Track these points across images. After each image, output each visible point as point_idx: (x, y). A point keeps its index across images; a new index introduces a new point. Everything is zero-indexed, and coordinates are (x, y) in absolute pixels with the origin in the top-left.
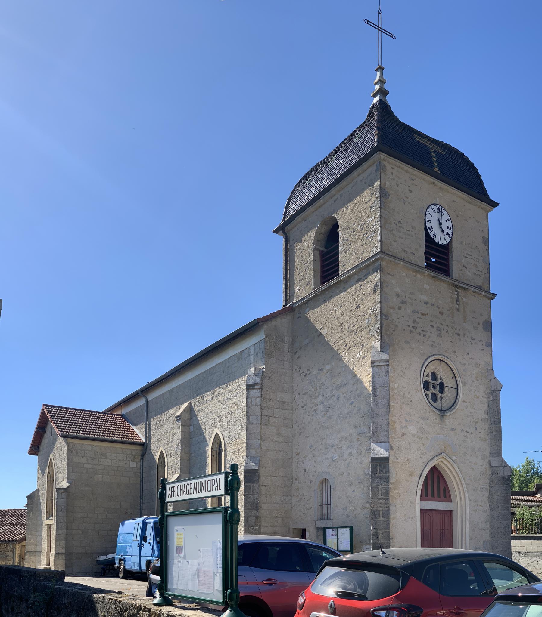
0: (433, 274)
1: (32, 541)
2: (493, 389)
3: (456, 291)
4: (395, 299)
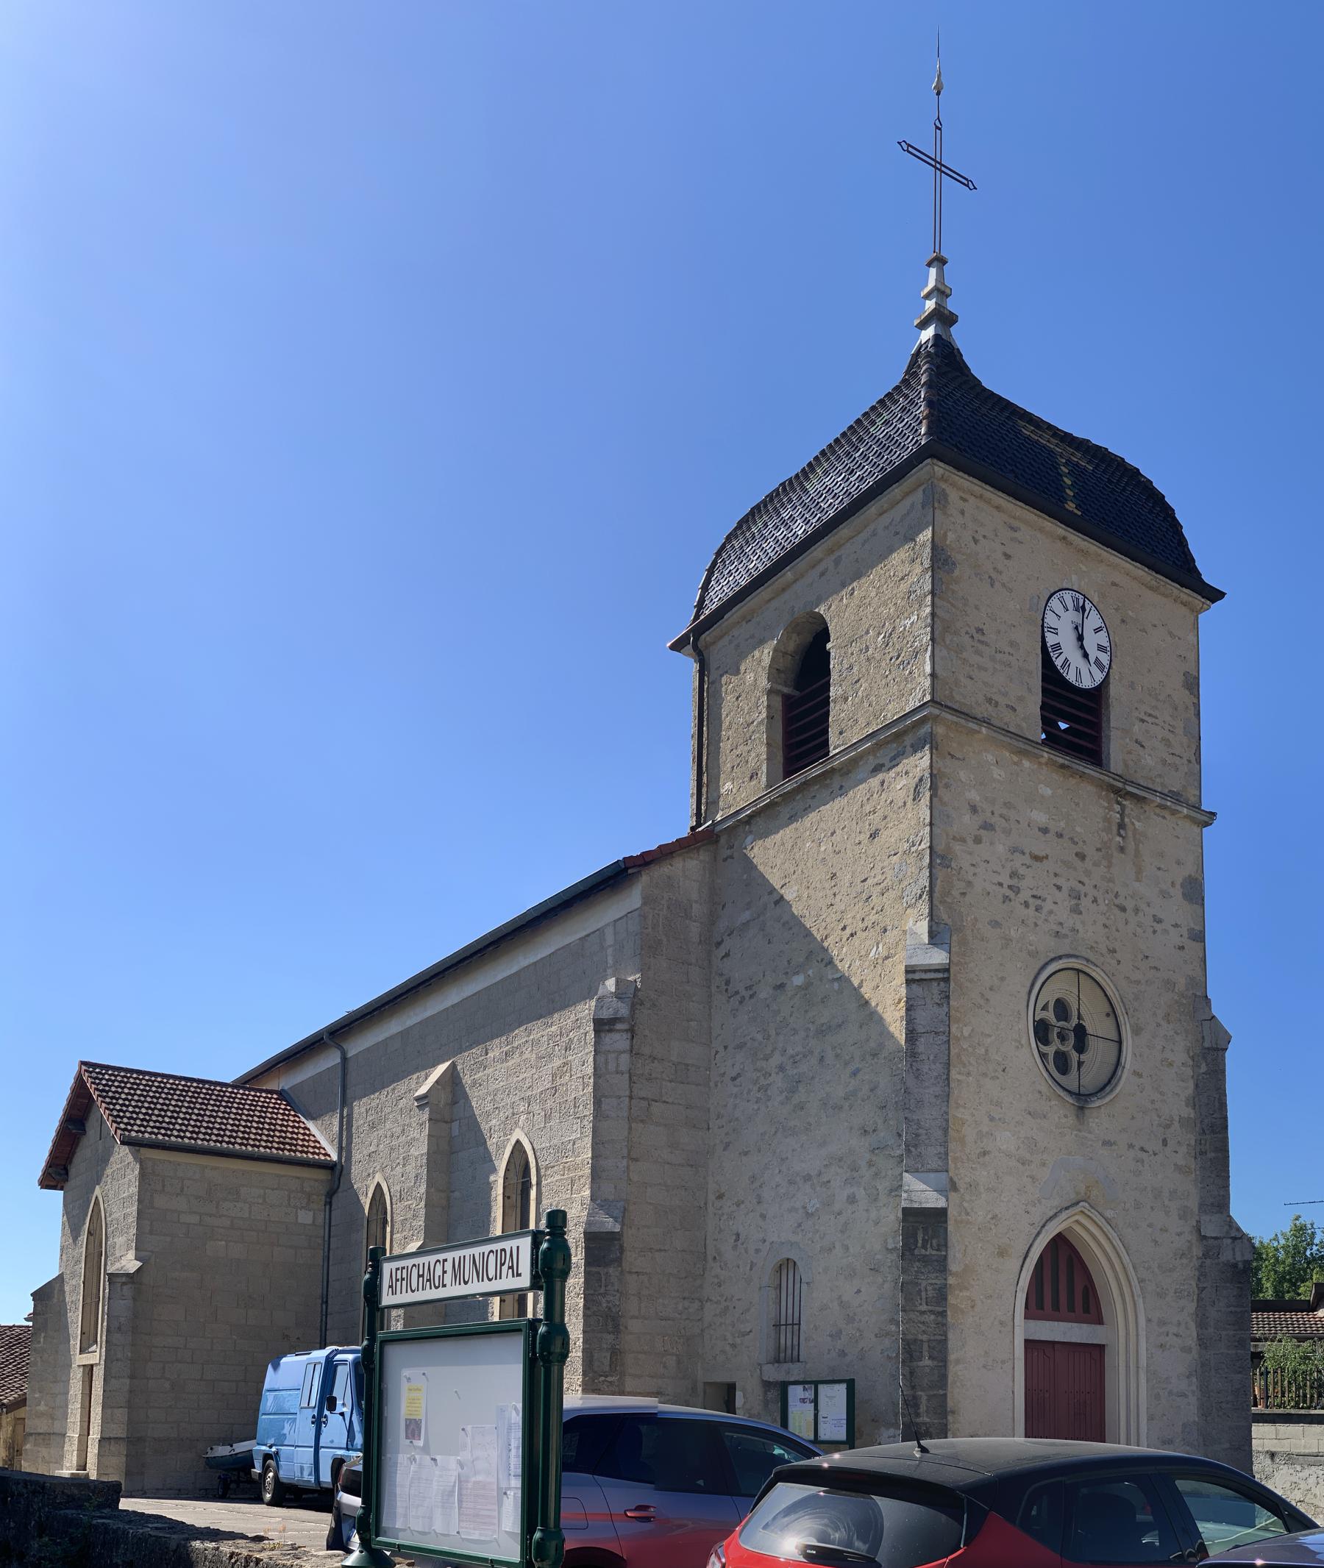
1: (42, 1408)
2: (1207, 1045)
3: (1118, 803)
4: (967, 818)
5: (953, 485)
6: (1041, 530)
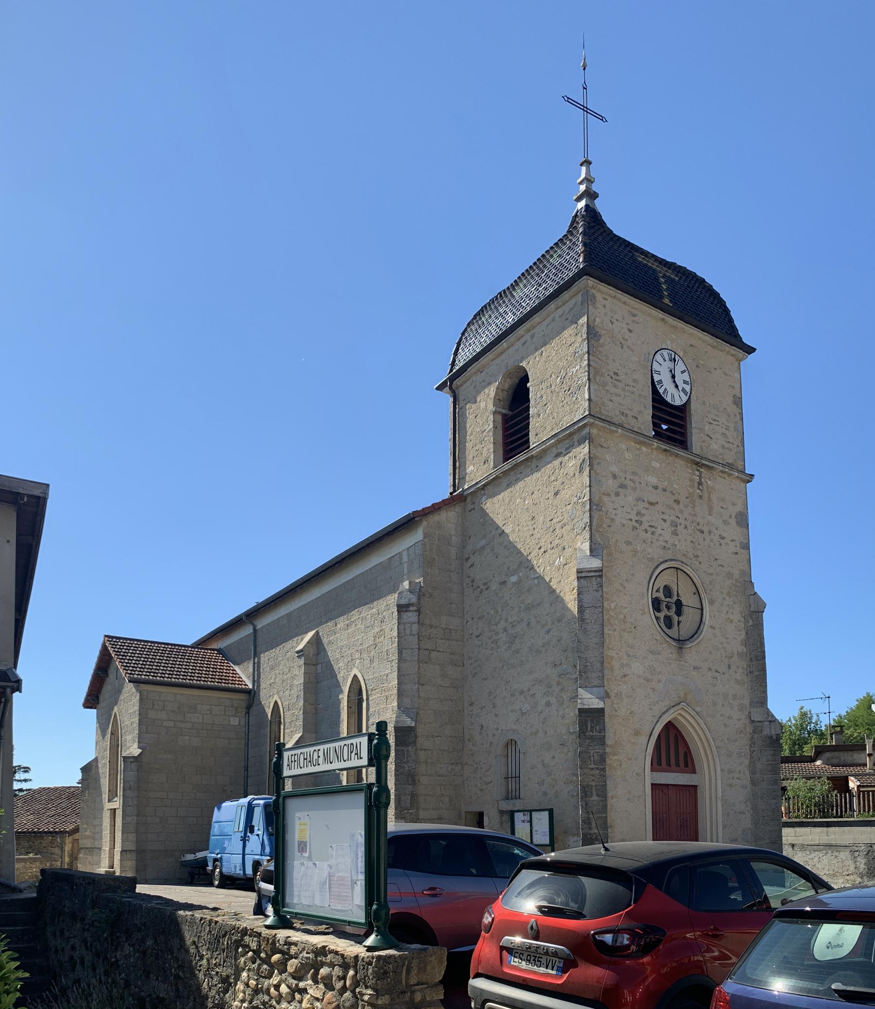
0: (664, 447)
1: (88, 833)
2: (752, 609)
3: (698, 470)
4: (610, 482)
5: (599, 291)
6: (650, 315)
